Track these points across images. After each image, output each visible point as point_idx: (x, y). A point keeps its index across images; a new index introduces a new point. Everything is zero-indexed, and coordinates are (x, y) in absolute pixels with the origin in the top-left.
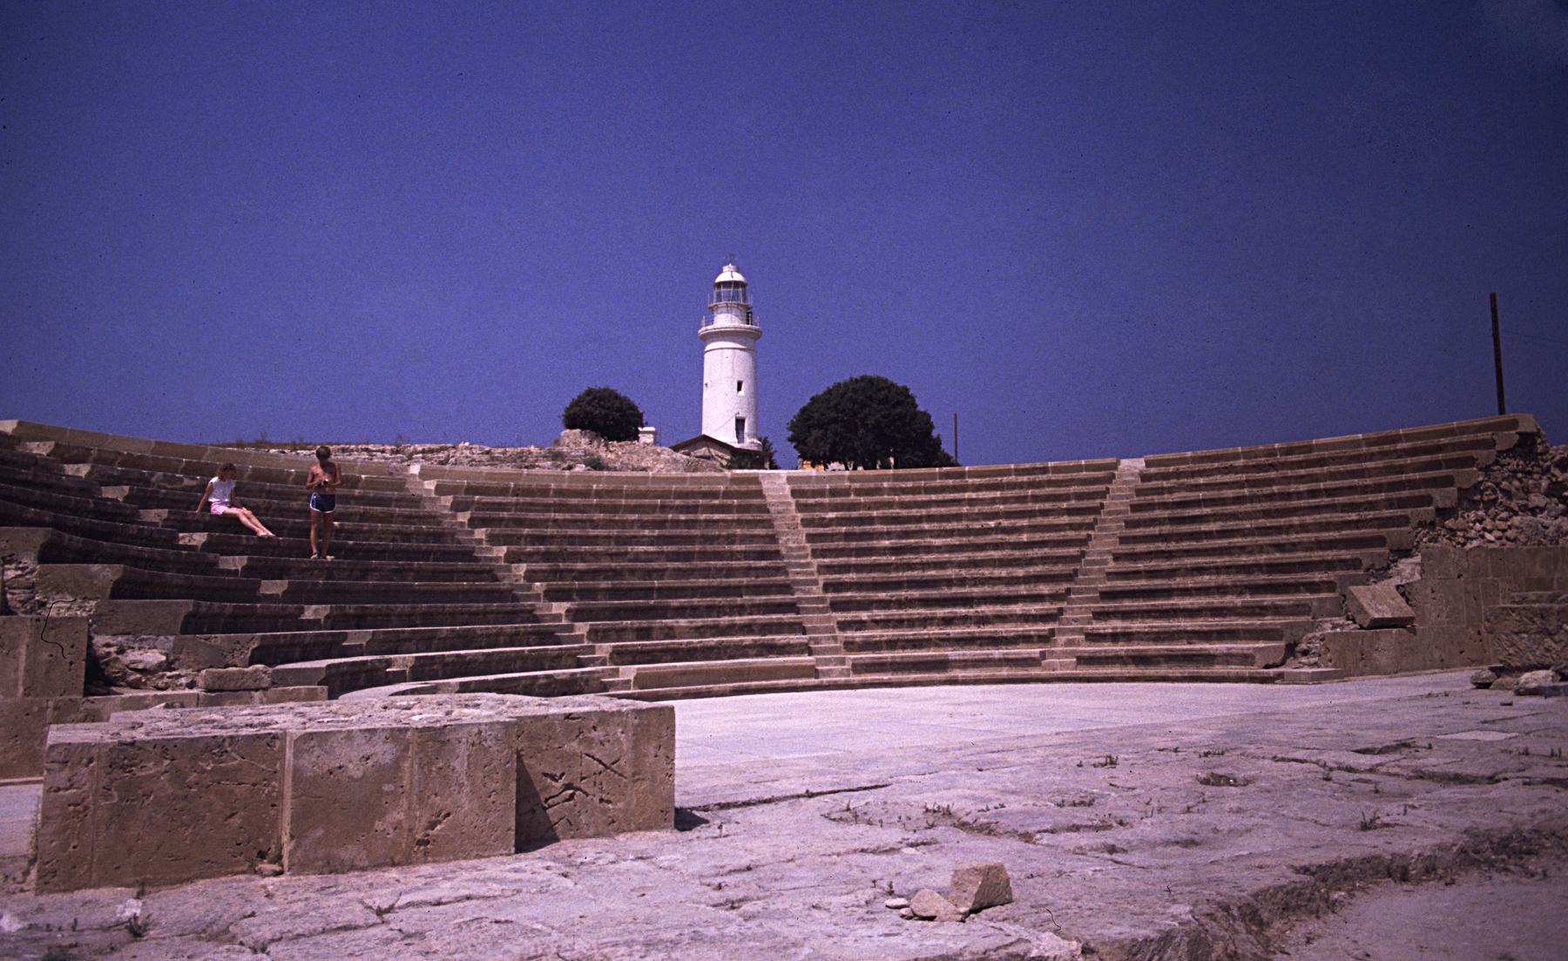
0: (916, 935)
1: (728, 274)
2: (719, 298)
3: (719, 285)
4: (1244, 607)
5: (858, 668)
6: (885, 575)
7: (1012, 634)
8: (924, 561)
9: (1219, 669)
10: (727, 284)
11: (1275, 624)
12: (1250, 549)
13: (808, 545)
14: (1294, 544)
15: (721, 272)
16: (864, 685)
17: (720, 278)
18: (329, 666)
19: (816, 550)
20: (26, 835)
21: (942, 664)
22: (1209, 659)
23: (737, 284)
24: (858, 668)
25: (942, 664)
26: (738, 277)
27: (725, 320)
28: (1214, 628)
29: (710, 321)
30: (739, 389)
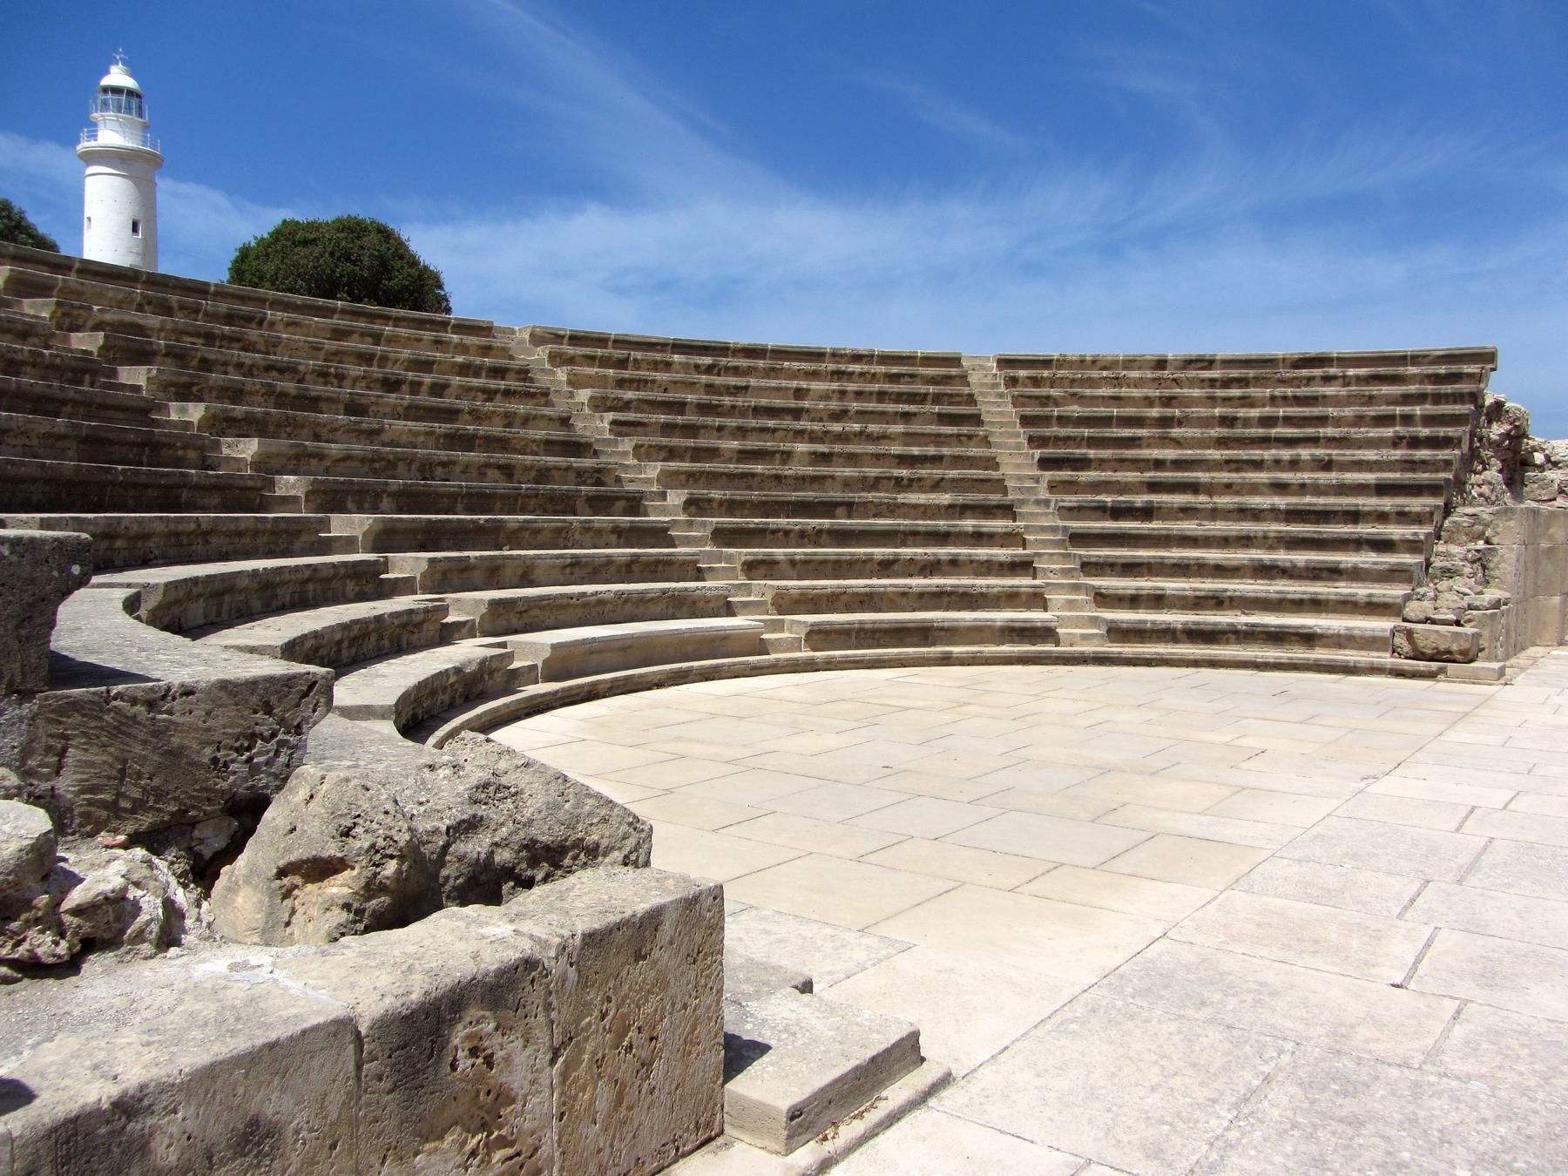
0: (1190, 1147)
1: (117, 77)
2: (105, 105)
3: (106, 90)
4: (1307, 569)
5: (819, 637)
6: (823, 494)
7: (996, 590)
8: (800, 473)
9: (1320, 654)
10: (117, 90)
11: (1268, 592)
12: (1238, 488)
13: (1022, 431)
14: (1303, 486)
15: (107, 72)
16: (830, 665)
17: (107, 81)
18: (171, 586)
19: (642, 446)
20: (748, 988)
21: (925, 634)
22: (1308, 639)
23: (131, 93)
24: (819, 637)
25: (925, 634)
26: (129, 82)
27: (112, 134)
28: (1289, 596)
29: (94, 136)
30: (135, 229)
